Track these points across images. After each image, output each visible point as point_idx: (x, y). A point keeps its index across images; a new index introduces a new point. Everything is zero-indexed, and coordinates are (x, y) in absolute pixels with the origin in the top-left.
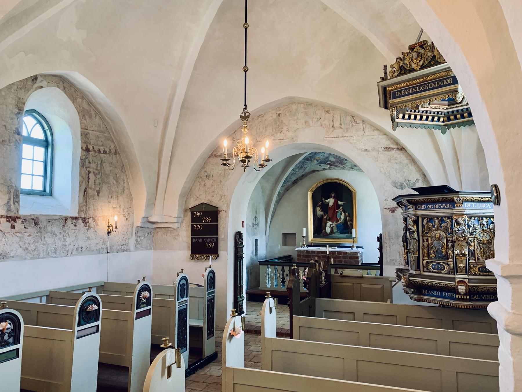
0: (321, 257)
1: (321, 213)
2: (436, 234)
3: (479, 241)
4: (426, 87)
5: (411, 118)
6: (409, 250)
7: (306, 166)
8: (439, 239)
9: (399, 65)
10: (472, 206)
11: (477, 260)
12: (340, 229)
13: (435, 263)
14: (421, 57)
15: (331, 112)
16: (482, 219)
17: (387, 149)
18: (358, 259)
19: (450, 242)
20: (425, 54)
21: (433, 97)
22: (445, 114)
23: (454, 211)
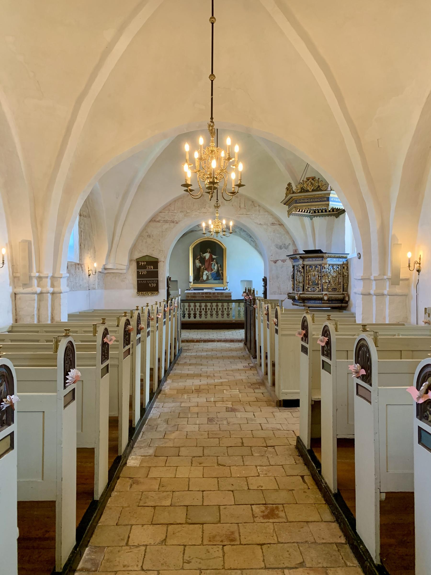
14: (313, 185)
15: (239, 197)
17: (273, 224)
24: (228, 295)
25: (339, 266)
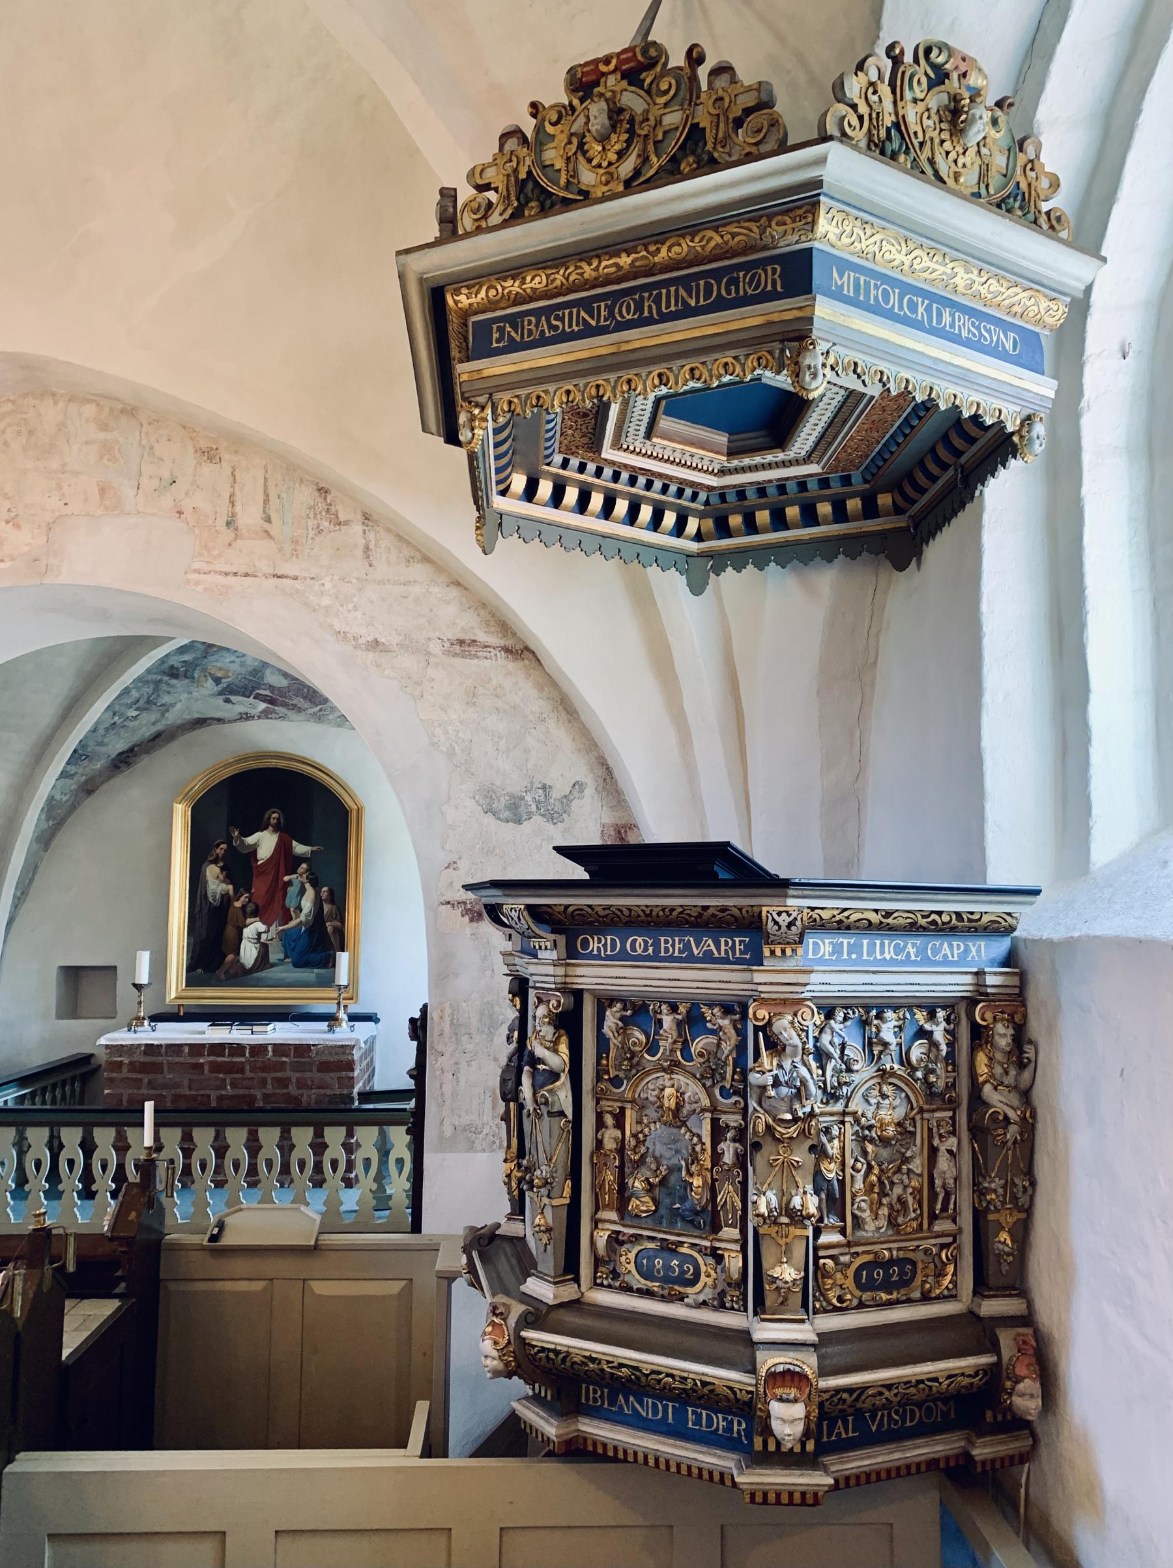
0: (206, 1068)
1: (224, 886)
2: (662, 1090)
3: (862, 1128)
4: (646, 304)
5: (564, 502)
6: (528, 1170)
7: (166, 699)
8: (677, 1117)
9: (516, 171)
10: (841, 953)
11: (854, 1228)
12: (293, 950)
13: (651, 1245)
15: (226, 456)
16: (879, 1016)
17: (464, 646)
18: (353, 1070)
19: (729, 1135)
20: (652, 118)
21: (679, 362)
22: (707, 503)
23: (756, 981)
24: (336, 1058)
25: (932, 1016)
